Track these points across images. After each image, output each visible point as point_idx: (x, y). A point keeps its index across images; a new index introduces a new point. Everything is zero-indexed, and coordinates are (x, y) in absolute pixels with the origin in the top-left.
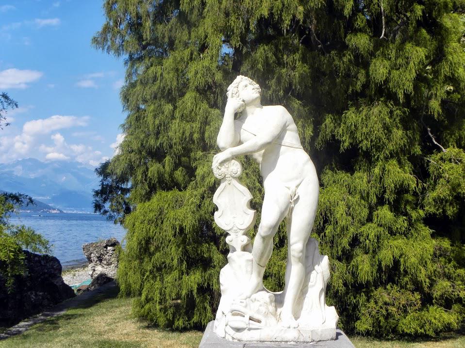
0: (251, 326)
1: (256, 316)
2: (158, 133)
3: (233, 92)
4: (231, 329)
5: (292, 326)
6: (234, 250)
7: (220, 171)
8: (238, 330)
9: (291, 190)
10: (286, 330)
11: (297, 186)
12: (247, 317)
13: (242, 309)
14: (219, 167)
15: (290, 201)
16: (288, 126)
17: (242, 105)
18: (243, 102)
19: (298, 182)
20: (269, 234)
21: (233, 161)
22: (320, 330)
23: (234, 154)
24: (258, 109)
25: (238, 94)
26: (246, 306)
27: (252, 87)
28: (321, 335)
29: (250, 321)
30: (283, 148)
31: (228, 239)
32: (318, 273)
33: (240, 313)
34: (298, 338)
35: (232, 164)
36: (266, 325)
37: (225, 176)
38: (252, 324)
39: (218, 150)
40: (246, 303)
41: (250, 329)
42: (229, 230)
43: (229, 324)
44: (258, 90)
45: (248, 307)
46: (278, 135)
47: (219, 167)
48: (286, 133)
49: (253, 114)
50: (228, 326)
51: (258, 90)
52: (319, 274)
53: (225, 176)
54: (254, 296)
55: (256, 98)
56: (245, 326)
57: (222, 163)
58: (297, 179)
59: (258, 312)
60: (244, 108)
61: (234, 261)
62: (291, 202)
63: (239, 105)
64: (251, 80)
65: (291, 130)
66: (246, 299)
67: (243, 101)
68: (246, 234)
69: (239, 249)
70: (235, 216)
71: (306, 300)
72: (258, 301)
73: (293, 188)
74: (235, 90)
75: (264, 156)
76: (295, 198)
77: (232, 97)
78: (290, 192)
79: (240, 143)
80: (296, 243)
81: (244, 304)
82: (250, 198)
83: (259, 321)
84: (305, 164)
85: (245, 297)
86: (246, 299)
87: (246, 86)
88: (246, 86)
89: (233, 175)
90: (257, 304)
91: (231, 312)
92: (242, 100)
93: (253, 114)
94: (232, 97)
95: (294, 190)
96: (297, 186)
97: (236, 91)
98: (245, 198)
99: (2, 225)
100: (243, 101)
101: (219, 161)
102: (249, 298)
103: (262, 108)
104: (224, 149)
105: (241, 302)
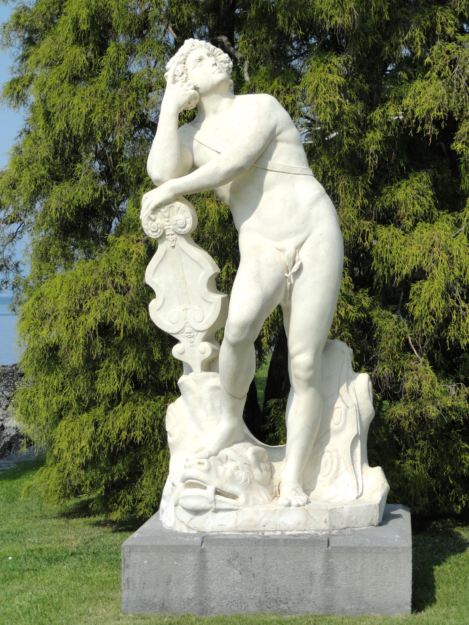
0: (219, 506)
1: (229, 488)
2: (121, 125)
3: (176, 73)
4: (184, 511)
5: (294, 503)
6: (191, 371)
7: (154, 224)
8: (197, 512)
9: (287, 253)
10: (282, 511)
11: (299, 247)
12: (210, 490)
13: (202, 476)
14: (153, 217)
15: (286, 275)
16: (279, 134)
17: (193, 98)
18: (194, 91)
19: (298, 239)
20: (243, 337)
21: (178, 204)
22: (346, 509)
23: (178, 191)
24: (225, 101)
25: (184, 76)
26: (209, 470)
27: (212, 60)
28: (349, 517)
29: (217, 496)
30: (269, 176)
31: (176, 351)
32: (348, 407)
33: (202, 483)
34: (306, 524)
35: (175, 209)
36: (247, 502)
37: (164, 232)
38: (220, 501)
39: (151, 186)
40: (210, 464)
41: (216, 511)
42: (178, 333)
43: (181, 502)
44: (227, 65)
45: (213, 471)
46: (259, 151)
47: (153, 217)
48: (276, 146)
49: (215, 112)
50: (179, 507)
51: (227, 65)
52: (350, 409)
53: (164, 232)
54: (227, 452)
55: (222, 81)
56: (209, 506)
57: (157, 209)
58: (296, 232)
59: (233, 479)
60: (197, 101)
61: (188, 389)
62: (286, 277)
63: (186, 98)
64: (212, 47)
65: (287, 141)
66: (209, 457)
67: (196, 88)
68: (206, 339)
69: (197, 367)
70: (188, 307)
71: (326, 457)
72: (232, 461)
73: (290, 251)
74: (180, 68)
75: (233, 191)
76: (295, 269)
77: (174, 82)
78: (284, 258)
79: (194, 167)
80: (299, 353)
81: (205, 467)
82: (212, 272)
83: (234, 497)
84: (316, 201)
85: (207, 455)
86: (209, 457)
87: (200, 60)
88: (200, 60)
89: (179, 230)
90: (230, 466)
91: (184, 482)
92: (192, 86)
93: (215, 112)
94: (174, 82)
95: (292, 255)
96: (299, 247)
97: (181, 70)
98: (203, 272)
99: (387, 622)
100: (196, 88)
101: (152, 206)
102: (216, 454)
103: (234, 98)
104: (161, 182)
105: (199, 463)
